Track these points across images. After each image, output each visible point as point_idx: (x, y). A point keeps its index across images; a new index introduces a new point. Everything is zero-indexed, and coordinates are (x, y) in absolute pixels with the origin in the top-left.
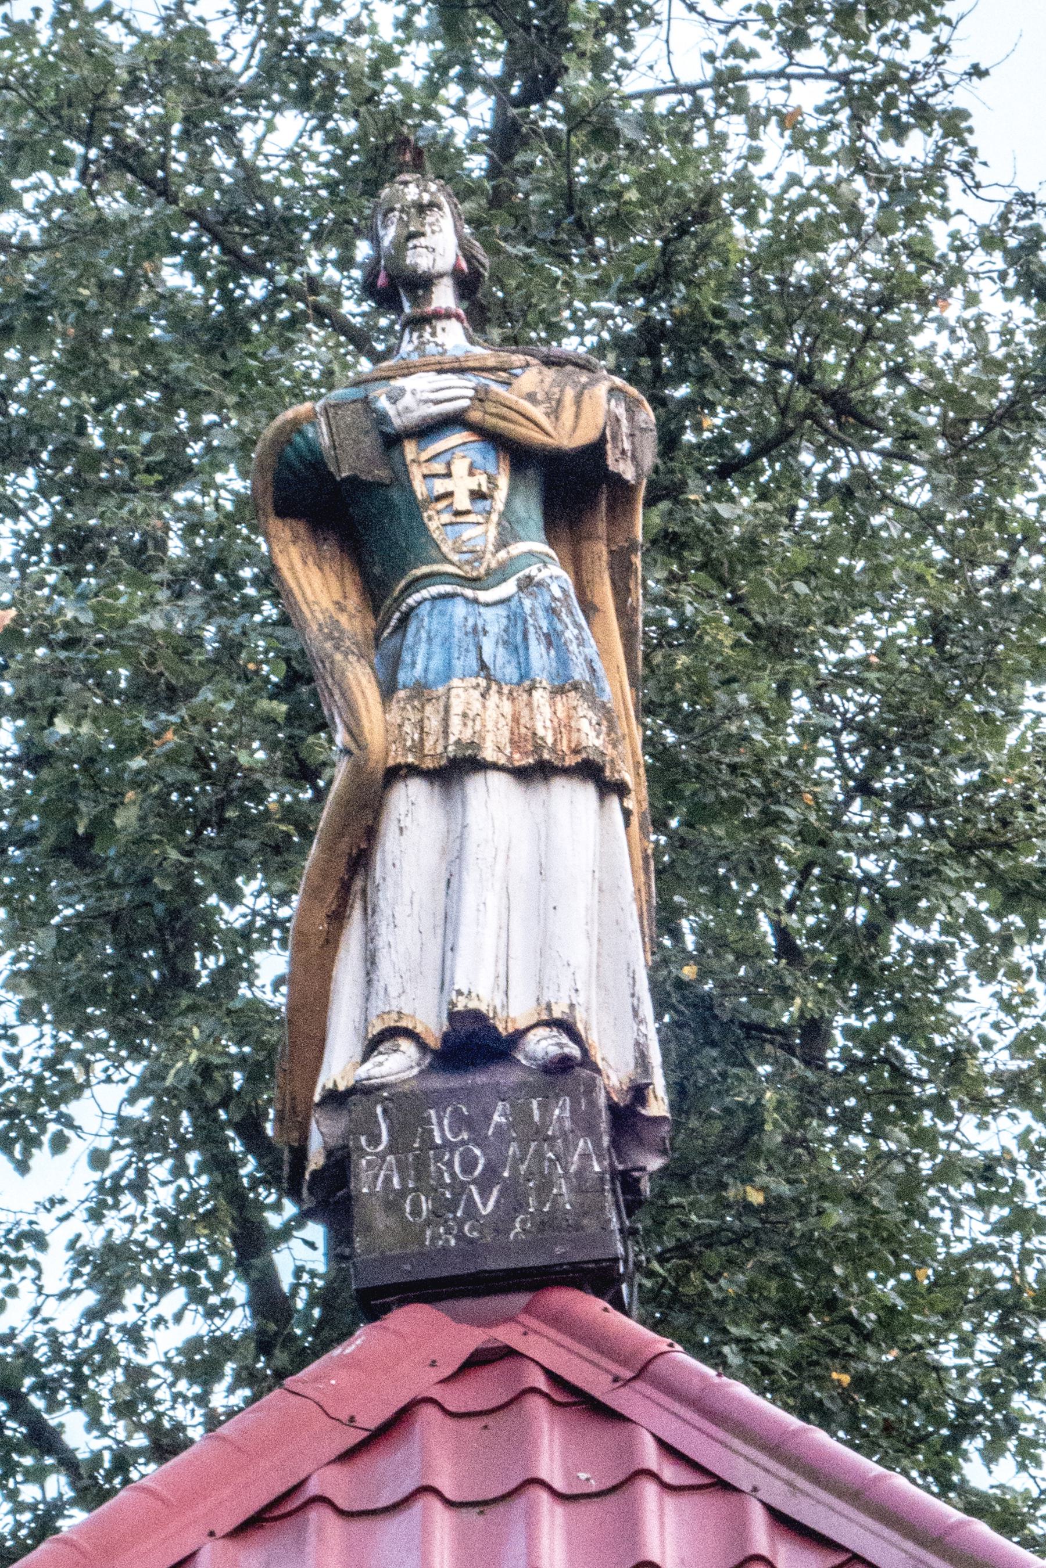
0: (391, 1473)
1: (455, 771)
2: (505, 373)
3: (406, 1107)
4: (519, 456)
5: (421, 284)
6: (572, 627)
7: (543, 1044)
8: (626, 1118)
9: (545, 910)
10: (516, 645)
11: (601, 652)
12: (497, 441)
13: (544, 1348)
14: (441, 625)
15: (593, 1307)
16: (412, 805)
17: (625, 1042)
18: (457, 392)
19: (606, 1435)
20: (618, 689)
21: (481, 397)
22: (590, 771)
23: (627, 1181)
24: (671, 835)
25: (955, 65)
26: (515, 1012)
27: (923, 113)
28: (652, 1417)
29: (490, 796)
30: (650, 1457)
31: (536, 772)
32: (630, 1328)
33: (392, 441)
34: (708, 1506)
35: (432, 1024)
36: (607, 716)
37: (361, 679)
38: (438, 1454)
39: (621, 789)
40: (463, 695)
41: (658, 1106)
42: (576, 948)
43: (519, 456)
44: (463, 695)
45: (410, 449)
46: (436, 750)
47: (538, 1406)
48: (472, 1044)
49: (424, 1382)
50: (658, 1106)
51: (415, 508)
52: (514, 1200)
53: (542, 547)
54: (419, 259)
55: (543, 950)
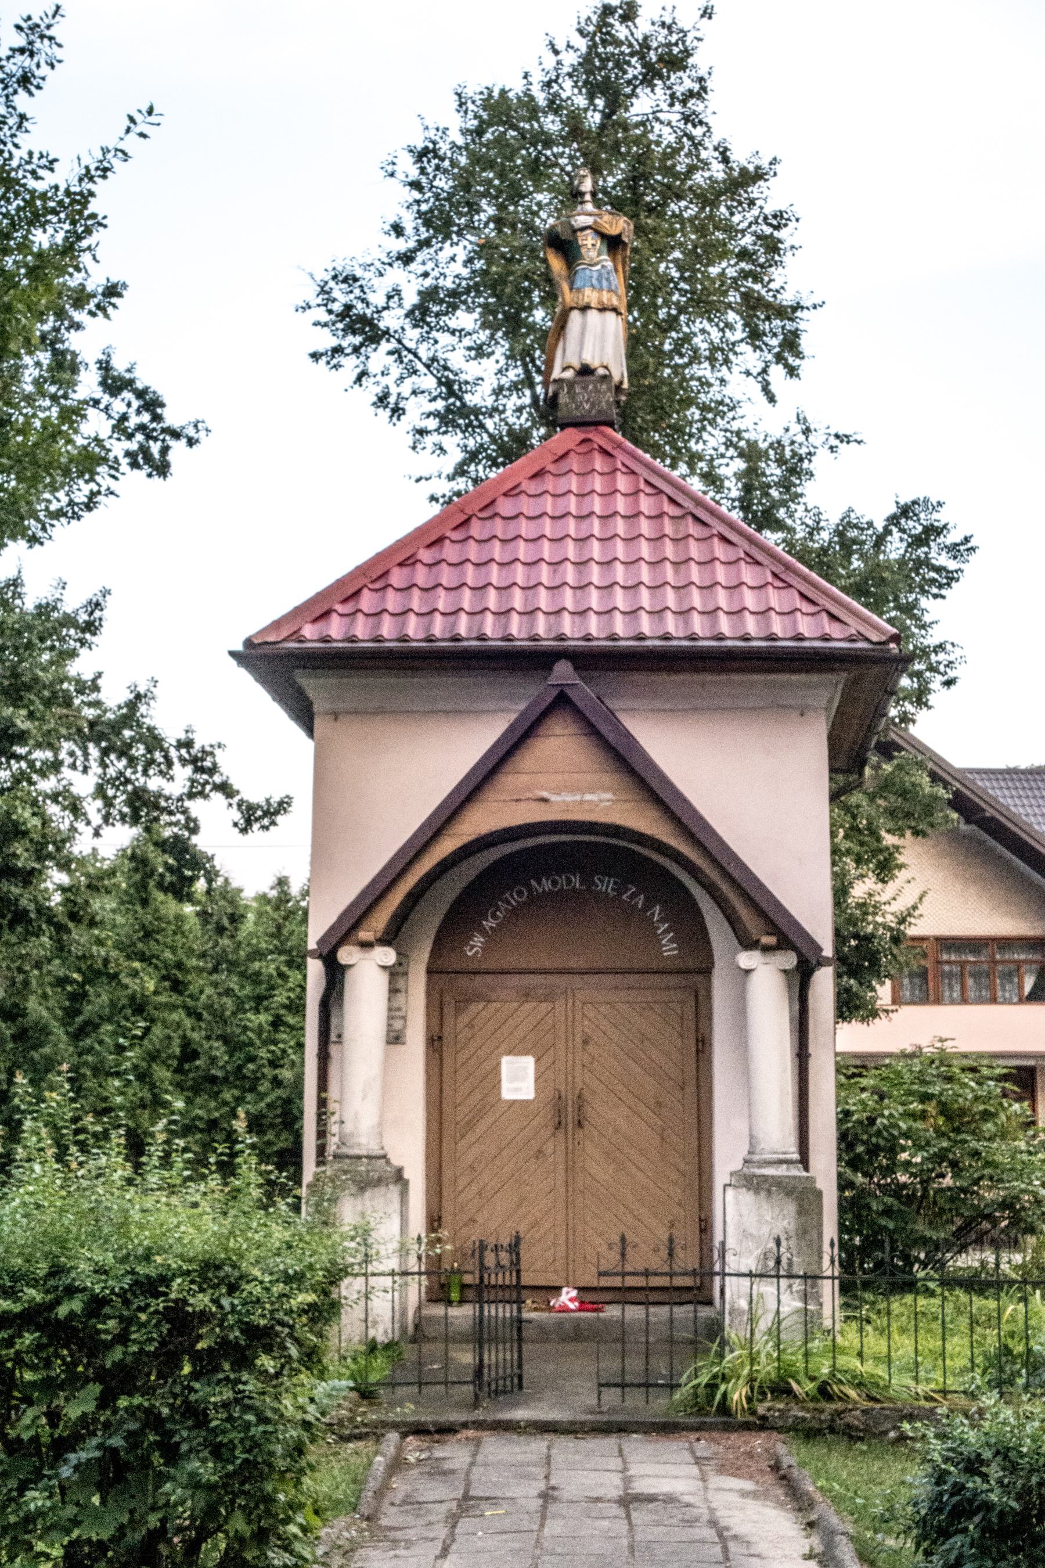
0: (564, 466)
1: (585, 309)
2: (600, 216)
3: (571, 384)
5: (582, 194)
6: (613, 277)
7: (601, 371)
8: (618, 388)
9: (603, 340)
10: (599, 280)
11: (618, 281)
13: (599, 440)
14: (586, 273)
15: (609, 431)
16: (575, 316)
17: (619, 371)
18: (589, 221)
19: (609, 460)
20: (622, 290)
22: (615, 310)
23: (618, 402)
25: (709, 111)
26: (595, 363)
27: (701, 123)
28: (621, 457)
29: (593, 315)
30: (619, 466)
31: (602, 309)
32: (619, 436)
33: (574, 231)
34: (631, 478)
35: (577, 366)
36: (619, 297)
37: (565, 287)
38: (574, 463)
40: (588, 291)
41: (626, 386)
42: (610, 350)
43: (603, 236)
44: (588, 291)
46: (581, 304)
48: (585, 371)
50: (626, 386)
51: (579, 247)
52: (593, 405)
54: (583, 189)
55: (602, 349)
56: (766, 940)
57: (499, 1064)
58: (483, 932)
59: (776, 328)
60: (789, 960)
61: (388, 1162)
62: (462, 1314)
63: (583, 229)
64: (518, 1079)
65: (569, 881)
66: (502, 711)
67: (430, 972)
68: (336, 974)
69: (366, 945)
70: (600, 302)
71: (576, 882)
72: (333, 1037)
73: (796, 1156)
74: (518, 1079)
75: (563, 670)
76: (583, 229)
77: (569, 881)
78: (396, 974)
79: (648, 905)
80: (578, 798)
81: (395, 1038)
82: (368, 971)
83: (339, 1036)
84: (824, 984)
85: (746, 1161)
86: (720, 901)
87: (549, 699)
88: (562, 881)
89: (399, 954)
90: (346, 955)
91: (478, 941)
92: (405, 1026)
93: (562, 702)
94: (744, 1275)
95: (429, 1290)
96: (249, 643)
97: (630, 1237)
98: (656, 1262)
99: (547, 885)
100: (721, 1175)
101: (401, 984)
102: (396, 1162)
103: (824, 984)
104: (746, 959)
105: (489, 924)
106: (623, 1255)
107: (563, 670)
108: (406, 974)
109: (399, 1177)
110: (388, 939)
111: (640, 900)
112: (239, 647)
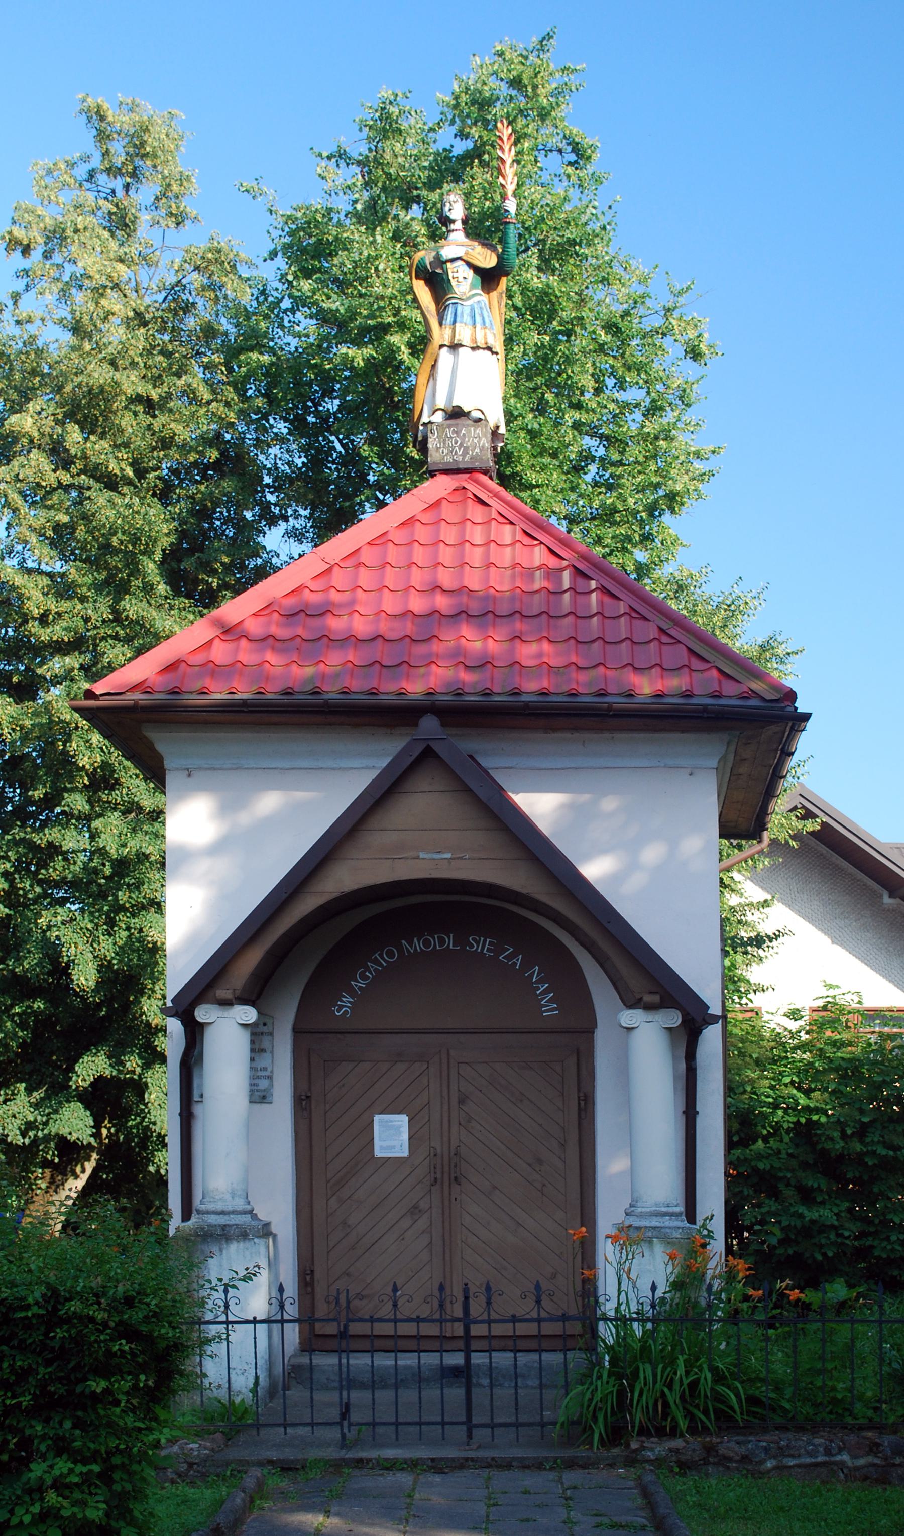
4: (477, 270)
12: (470, 265)
13: (472, 487)
18: (459, 252)
21: (467, 253)
24: (70, 1335)
39: (497, 353)
45: (449, 264)
47: (470, 501)
48: (456, 414)
49: (444, 493)
53: (480, 292)
56: (647, 998)
57: (371, 1123)
58: (351, 992)
60: (674, 1019)
61: (254, 1217)
62: (326, 1361)
63: (453, 260)
64: (392, 1135)
65: (442, 941)
66: (367, 768)
67: (298, 1031)
68: (195, 1033)
69: (226, 1003)
71: (450, 942)
72: (196, 1098)
73: (681, 1209)
74: (392, 1135)
75: (429, 724)
76: (453, 260)
77: (442, 941)
78: (258, 1035)
79: (527, 965)
81: (259, 1096)
82: (228, 1030)
83: (202, 1096)
86: (601, 960)
87: (416, 753)
88: (434, 941)
90: (202, 1014)
91: (347, 1000)
92: (272, 1085)
93: (426, 756)
94: (247, 1322)
97: (545, 1285)
98: (527, 1308)
99: (418, 945)
101: (266, 1043)
104: (631, 1017)
105: (359, 984)
106: (489, 1303)
107: (429, 724)
108: (271, 1034)
109: (266, 1231)
110: (250, 996)
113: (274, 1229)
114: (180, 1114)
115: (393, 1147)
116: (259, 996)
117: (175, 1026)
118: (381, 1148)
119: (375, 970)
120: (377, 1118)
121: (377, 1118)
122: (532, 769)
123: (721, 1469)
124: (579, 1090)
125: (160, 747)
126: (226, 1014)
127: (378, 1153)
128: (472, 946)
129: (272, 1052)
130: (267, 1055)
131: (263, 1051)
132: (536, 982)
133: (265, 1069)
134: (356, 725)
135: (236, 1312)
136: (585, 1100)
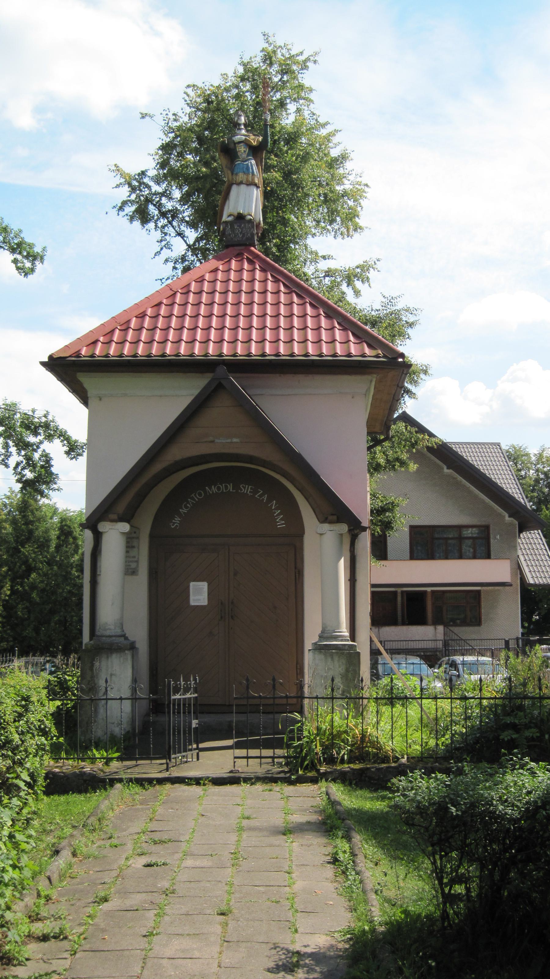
16: (234, 188)
33: (235, 143)
48: (240, 217)
56: (331, 518)
58: (180, 515)
59: (340, 212)
60: (344, 528)
61: (126, 638)
64: (199, 594)
65: (226, 487)
67: (152, 537)
68: (98, 536)
70: (247, 181)
71: (230, 487)
74: (199, 594)
75: (222, 370)
79: (269, 500)
80: (229, 441)
81: (130, 571)
84: (365, 541)
85: (320, 637)
86: (292, 481)
88: (222, 487)
89: (132, 526)
91: (177, 520)
92: (138, 565)
95: (116, 736)
96: (51, 357)
100: (308, 645)
102: (131, 639)
103: (365, 541)
105: (183, 511)
107: (222, 370)
108: (138, 538)
109: (132, 647)
110: (126, 517)
111: (265, 498)
112: (46, 360)
113: (137, 645)
114: (90, 582)
115: (199, 600)
116: (133, 516)
117: (88, 534)
118: (194, 600)
119: (192, 503)
120: (192, 584)
121: (192, 584)
122: (272, 395)
123: (365, 713)
124: (296, 568)
125: (86, 386)
126: (113, 527)
127: (192, 603)
128: (241, 490)
129: (138, 548)
130: (136, 550)
131: (133, 547)
132: (274, 509)
133: (134, 557)
134: (185, 372)
135: (111, 695)
136: (299, 573)
